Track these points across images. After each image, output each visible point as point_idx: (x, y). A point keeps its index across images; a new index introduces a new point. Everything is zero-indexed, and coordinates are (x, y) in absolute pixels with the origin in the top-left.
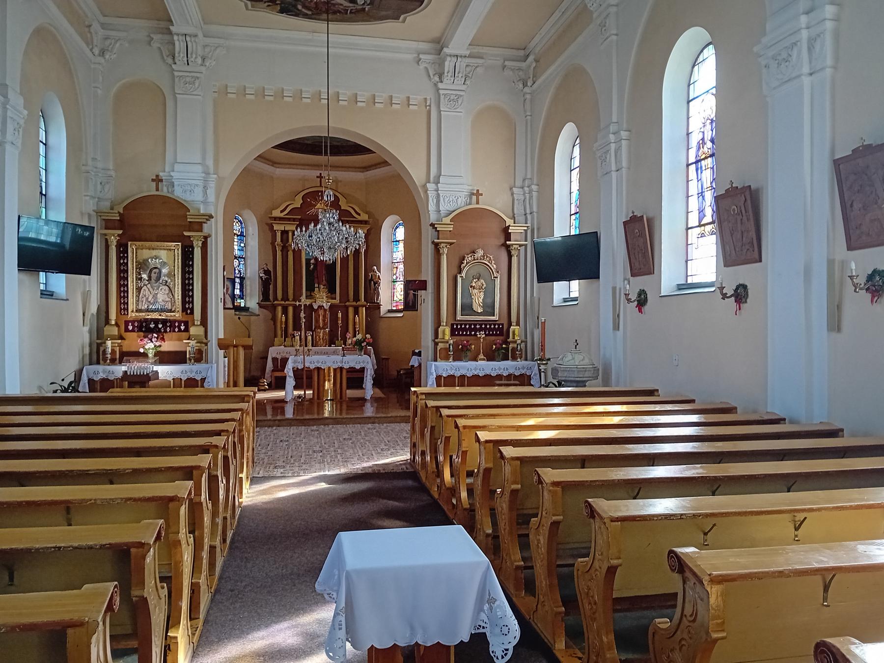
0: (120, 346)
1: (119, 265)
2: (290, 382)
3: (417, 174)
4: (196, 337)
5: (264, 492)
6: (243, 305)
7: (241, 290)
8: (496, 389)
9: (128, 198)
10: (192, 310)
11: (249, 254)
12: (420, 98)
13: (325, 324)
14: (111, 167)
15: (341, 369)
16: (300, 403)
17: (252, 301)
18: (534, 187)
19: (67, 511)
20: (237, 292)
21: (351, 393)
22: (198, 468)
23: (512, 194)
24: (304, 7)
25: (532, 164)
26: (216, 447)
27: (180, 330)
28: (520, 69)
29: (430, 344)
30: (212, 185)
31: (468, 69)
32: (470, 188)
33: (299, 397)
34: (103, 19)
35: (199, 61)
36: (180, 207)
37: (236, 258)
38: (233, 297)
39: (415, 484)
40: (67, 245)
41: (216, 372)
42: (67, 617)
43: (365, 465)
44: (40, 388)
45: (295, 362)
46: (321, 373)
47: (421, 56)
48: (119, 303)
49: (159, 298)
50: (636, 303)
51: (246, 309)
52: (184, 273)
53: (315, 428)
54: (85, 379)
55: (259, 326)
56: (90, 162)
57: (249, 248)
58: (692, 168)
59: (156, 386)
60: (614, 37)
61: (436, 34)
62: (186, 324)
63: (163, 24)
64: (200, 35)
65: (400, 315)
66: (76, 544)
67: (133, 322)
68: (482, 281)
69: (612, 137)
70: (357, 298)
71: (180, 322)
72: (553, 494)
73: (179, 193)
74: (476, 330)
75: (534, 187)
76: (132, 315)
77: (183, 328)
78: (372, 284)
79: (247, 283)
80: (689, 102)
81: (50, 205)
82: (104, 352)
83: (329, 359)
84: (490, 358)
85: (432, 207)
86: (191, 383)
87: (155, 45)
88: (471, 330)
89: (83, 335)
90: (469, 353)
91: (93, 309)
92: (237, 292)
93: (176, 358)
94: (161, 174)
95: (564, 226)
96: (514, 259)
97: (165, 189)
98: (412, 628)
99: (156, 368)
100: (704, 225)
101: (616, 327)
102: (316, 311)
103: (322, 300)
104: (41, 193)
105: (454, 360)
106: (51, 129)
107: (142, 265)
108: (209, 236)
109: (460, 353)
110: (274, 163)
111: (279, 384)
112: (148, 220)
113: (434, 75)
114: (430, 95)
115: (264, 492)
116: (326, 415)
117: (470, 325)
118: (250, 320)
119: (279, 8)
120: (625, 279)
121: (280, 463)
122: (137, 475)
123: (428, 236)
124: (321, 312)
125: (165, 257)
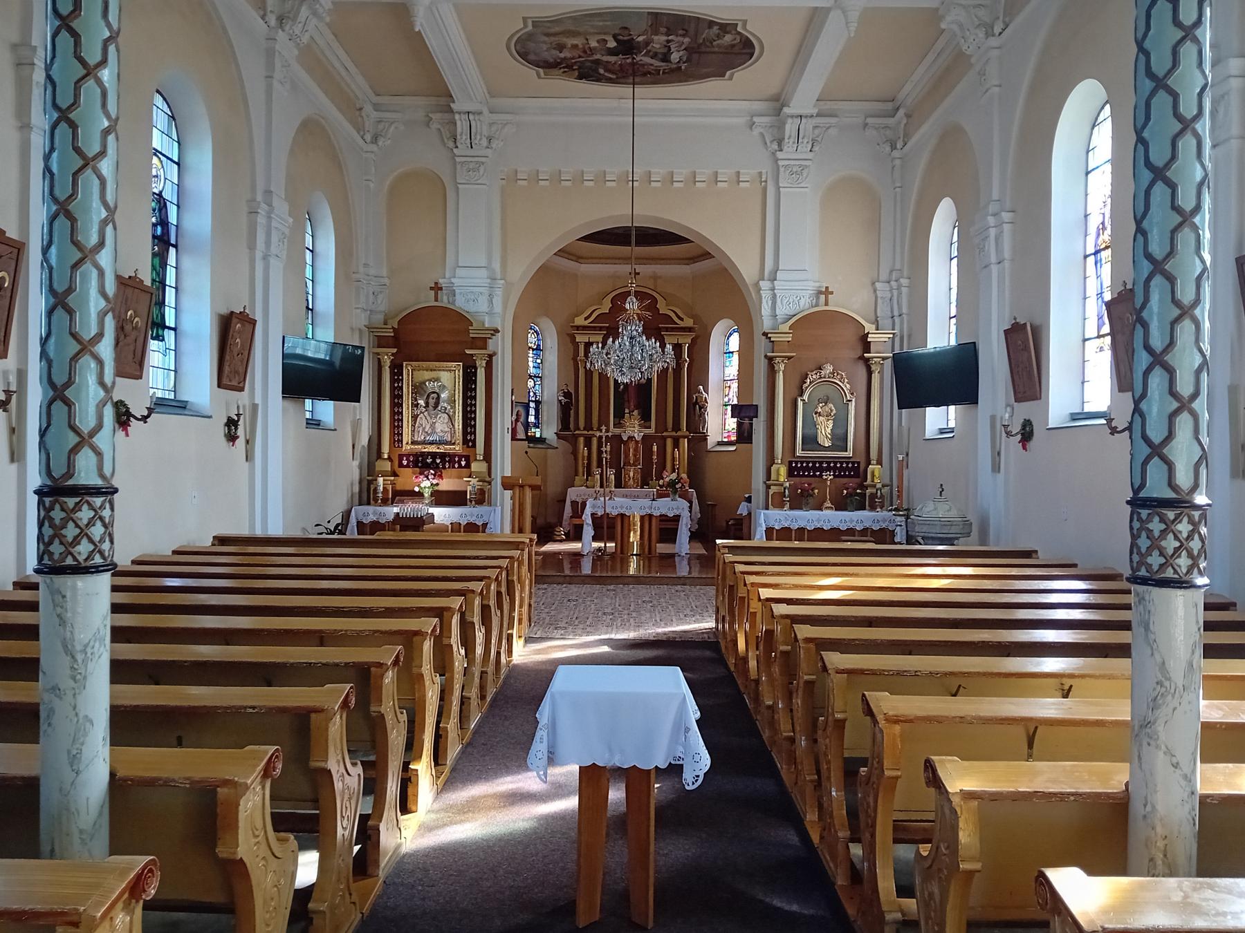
0: (393, 484)
1: (393, 389)
2: (588, 532)
3: (747, 269)
4: (478, 475)
5: (539, 652)
6: (538, 435)
7: (537, 417)
8: (848, 545)
9: (401, 312)
10: (474, 442)
11: (546, 372)
12: (754, 172)
13: (636, 460)
14: (385, 274)
15: (650, 516)
16: (599, 556)
17: (549, 431)
18: (904, 282)
19: (321, 638)
20: (532, 419)
21: (662, 548)
22: (448, 609)
23: (875, 291)
24: (607, 70)
25: (903, 247)
26: (473, 591)
27: (460, 466)
28: (886, 127)
29: (762, 488)
30: (499, 292)
31: (817, 131)
32: (817, 284)
33: (599, 550)
34: (376, 99)
35: (485, 142)
36: (461, 320)
37: (530, 377)
38: (527, 426)
39: (714, 655)
40: (337, 363)
41: (500, 516)
42: (311, 704)
43: (660, 630)
44: (304, 529)
45: (594, 506)
46: (626, 521)
47: (755, 119)
48: (392, 434)
49: (438, 428)
50: (1019, 437)
51: (541, 440)
52: (465, 398)
53: (612, 587)
54: (353, 521)
55: (556, 461)
56: (361, 269)
57: (546, 364)
58: (1091, 260)
59: (432, 531)
60: (997, 89)
61: (773, 90)
62: (468, 459)
63: (443, 101)
64: (486, 111)
65: (733, 448)
66: (324, 661)
67: (408, 456)
68: (831, 405)
69: (991, 220)
70: (677, 427)
71: (461, 457)
72: (807, 650)
73: (461, 303)
74: (822, 470)
75: (904, 282)
76: (407, 448)
77: (463, 463)
78: (697, 409)
79: (544, 408)
80: (1087, 173)
81: (317, 321)
82: (375, 490)
83: (635, 505)
84: (840, 506)
85: (766, 310)
86: (471, 527)
87: (434, 126)
88: (814, 469)
89: (351, 470)
90: (811, 500)
91: (364, 441)
92: (532, 419)
93: (453, 499)
94: (441, 281)
95: (940, 336)
96: (876, 378)
97: (445, 298)
98: (610, 750)
99: (431, 510)
100: (1103, 336)
101: (996, 468)
102: (625, 443)
103: (634, 429)
104: (307, 308)
105: (791, 508)
106: (319, 234)
107: (418, 389)
108: (495, 354)
109: (799, 500)
110: (578, 258)
111: (576, 534)
112: (425, 336)
113: (772, 142)
114: (766, 169)
115: (539, 652)
116: (632, 572)
117: (814, 463)
118: (545, 456)
119: (576, 73)
120: (1008, 405)
121: (562, 624)
122: (390, 613)
123: (761, 347)
124: (632, 445)
125: (448, 379)
